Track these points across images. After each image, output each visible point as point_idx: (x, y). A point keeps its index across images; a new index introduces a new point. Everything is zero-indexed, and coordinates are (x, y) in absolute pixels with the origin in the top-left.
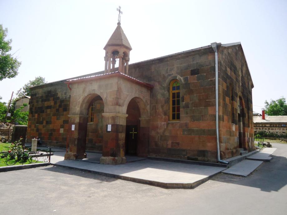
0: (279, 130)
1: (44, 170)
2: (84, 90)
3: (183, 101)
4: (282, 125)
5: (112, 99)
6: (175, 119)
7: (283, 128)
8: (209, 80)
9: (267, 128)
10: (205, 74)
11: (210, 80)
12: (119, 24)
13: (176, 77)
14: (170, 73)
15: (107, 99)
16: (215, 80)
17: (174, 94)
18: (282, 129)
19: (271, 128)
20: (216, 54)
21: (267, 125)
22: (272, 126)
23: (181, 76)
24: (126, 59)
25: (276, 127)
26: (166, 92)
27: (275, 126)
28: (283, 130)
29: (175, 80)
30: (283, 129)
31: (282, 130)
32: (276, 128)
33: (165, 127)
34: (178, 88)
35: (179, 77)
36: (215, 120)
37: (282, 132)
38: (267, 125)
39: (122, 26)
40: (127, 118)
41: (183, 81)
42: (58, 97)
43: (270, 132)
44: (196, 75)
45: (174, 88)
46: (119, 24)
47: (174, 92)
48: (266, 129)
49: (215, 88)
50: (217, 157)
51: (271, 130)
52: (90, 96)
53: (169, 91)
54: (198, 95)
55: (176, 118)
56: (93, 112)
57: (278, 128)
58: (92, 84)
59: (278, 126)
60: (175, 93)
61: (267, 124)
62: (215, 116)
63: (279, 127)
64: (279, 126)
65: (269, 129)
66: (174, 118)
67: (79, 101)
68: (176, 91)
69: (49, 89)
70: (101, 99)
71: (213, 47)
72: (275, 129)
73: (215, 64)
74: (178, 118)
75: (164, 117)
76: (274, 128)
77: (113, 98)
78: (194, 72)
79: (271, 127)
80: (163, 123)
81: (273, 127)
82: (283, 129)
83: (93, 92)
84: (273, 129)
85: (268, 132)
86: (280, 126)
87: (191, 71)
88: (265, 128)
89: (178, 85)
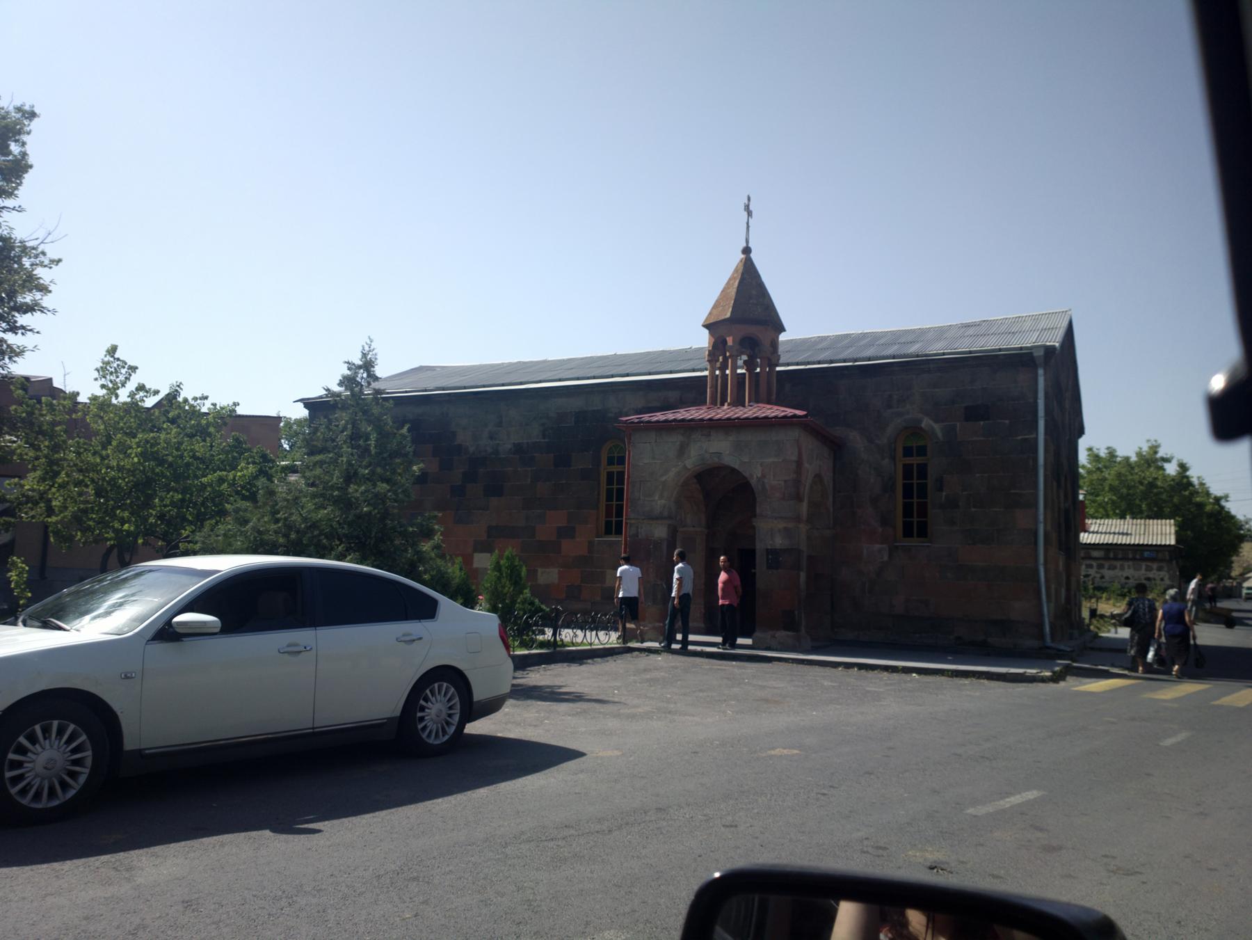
0: (1136, 569)
1: (607, 699)
2: (682, 451)
3: (941, 489)
4: (1146, 554)
5: (783, 483)
7: (1149, 564)
8: (1019, 438)
9: (1094, 564)
10: (1007, 422)
11: (1022, 439)
12: (747, 251)
13: (920, 421)
14: (898, 408)
15: (766, 481)
16: (1036, 439)
17: (908, 470)
18: (1144, 567)
19: (1107, 564)
20: (1041, 371)
21: (1095, 554)
22: (1112, 555)
23: (936, 421)
24: (1179, 473)
25: (1125, 559)
26: (886, 461)
27: (1120, 556)
28: (1146, 570)
29: (914, 430)
30: (1149, 569)
31: (1143, 571)
32: (1126, 564)
33: (886, 558)
34: (922, 451)
35: (926, 423)
36: (1036, 543)
37: (1143, 578)
38: (1095, 554)
39: (754, 256)
41: (940, 434)
42: (1125, 518)
43: (1102, 577)
44: (982, 423)
45: (908, 452)
46: (747, 251)
47: (908, 460)
48: (1090, 566)
49: (1036, 460)
50: (1041, 636)
51: (1109, 569)
53: (893, 458)
54: (986, 475)
56: (614, 519)
57: (1131, 563)
58: (709, 435)
59: (1130, 556)
60: (912, 465)
61: (1095, 549)
62: (1036, 534)
63: (1134, 559)
64: (657, 580)
65: (1100, 567)
66: (908, 532)
67: (664, 478)
68: (915, 460)
70: (1121, 518)
71: (1035, 354)
72: (1122, 568)
73: (1036, 398)
74: (923, 532)
75: (880, 530)
76: (1118, 564)
77: (785, 481)
78: (973, 414)
79: (1107, 558)
80: (877, 546)
81: (1115, 559)
82: (1147, 566)
83: (716, 460)
84: (1114, 568)
85: (1098, 576)
86: (1138, 557)
87: (966, 408)
88: (1088, 562)
89: (921, 443)
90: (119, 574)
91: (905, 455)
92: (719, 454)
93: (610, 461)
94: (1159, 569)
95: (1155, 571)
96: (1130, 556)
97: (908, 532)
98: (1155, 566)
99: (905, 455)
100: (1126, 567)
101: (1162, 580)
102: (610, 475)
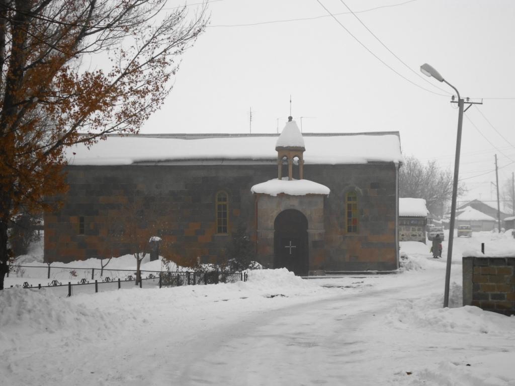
6: (351, 231)
7: (414, 227)
16: (395, 196)
17: (349, 206)
18: (411, 229)
30: (413, 230)
35: (357, 188)
40: (307, 229)
44: (376, 189)
45: (349, 199)
47: (220, 203)
52: (292, 208)
55: (352, 230)
57: (405, 227)
60: (351, 204)
63: (406, 225)
66: (349, 230)
68: (222, 203)
69: (295, 205)
78: (374, 186)
82: (413, 228)
86: (408, 223)
90: (388, 271)
91: (348, 200)
92: (294, 206)
93: (220, 200)
94: (419, 230)
95: (417, 231)
96: (405, 223)
97: (349, 230)
98: (417, 228)
99: (348, 200)
100: (402, 229)
101: (420, 236)
102: (219, 206)
